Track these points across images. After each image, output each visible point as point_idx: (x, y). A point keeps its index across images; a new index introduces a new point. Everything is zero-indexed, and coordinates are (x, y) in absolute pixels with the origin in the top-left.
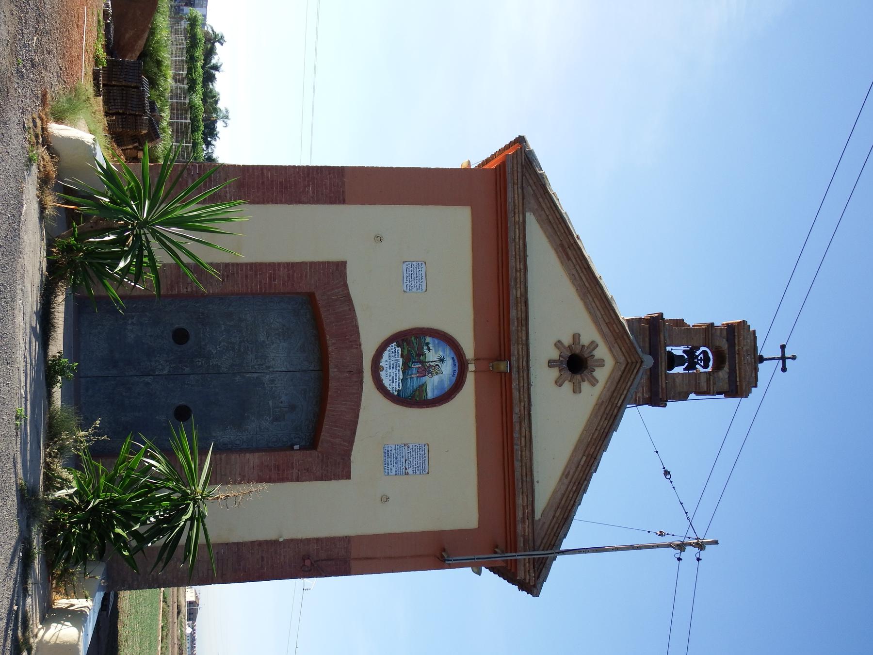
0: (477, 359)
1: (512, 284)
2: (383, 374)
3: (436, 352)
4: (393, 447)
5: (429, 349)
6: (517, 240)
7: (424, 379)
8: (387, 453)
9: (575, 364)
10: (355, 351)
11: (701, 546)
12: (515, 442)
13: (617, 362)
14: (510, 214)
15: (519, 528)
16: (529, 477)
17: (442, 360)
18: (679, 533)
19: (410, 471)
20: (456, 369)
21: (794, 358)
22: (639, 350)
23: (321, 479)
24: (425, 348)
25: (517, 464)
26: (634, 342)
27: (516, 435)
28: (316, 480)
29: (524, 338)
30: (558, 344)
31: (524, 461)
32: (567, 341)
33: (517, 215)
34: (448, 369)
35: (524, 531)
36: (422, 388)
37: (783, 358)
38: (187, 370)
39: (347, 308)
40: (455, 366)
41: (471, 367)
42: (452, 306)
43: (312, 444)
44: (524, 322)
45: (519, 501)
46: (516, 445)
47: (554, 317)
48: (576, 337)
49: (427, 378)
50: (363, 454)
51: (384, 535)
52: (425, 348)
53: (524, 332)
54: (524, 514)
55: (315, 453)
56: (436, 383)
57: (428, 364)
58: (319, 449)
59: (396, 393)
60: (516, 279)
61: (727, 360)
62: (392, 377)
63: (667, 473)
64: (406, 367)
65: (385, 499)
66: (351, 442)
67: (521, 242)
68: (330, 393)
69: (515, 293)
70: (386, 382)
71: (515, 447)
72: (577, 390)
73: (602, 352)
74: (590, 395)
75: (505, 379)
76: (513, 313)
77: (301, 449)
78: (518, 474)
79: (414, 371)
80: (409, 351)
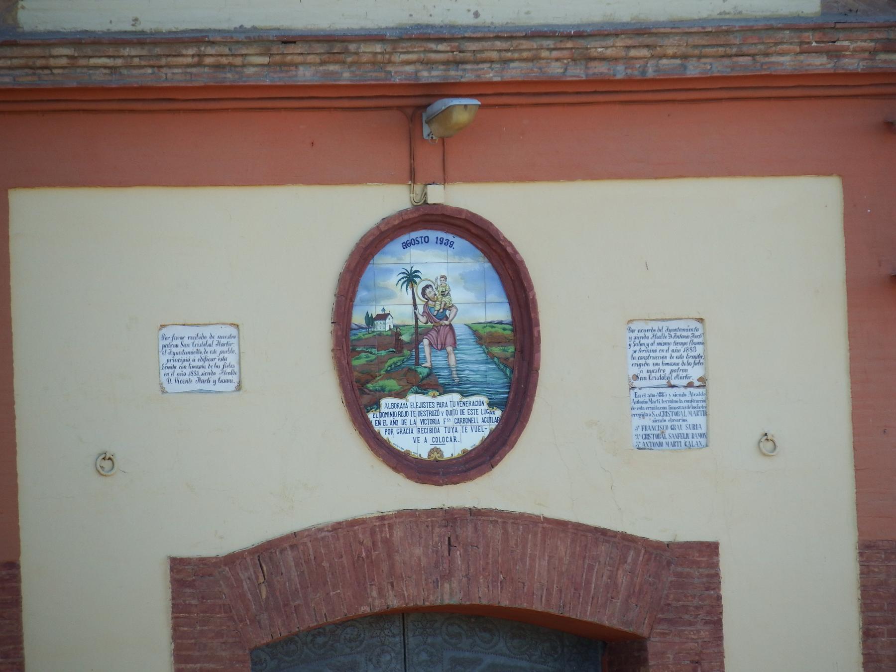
0: (412, 177)
1: (229, 77)
2: (450, 451)
3: (390, 296)
4: (637, 421)
5: (383, 317)
6: (119, 62)
7: (461, 332)
8: (651, 441)
10: (398, 533)
12: (636, 74)
14: (46, 80)
15: (852, 64)
16: (597, 48)
17: (411, 278)
19: (695, 373)
20: (433, 235)
23: (717, 624)
24: (381, 327)
25: (693, 69)
27: (620, 72)
28: (720, 638)
29: (378, 48)
31: (690, 51)
33: (52, 62)
34: (442, 263)
35: (863, 50)
36: (484, 337)
39: (290, 555)
40: (426, 240)
41: (437, 195)
44: (337, 48)
45: (785, 62)
46: (644, 72)
50: (651, 508)
51: (857, 447)
52: (381, 327)
53: (365, 48)
54: (818, 52)
55: (654, 645)
56: (470, 296)
57: (422, 320)
58: (644, 631)
59: (498, 413)
60: (218, 67)
62: (451, 424)
64: (429, 384)
65: (767, 443)
66: (627, 541)
67: (126, 51)
68: (505, 603)
69: (255, 68)
70: (471, 440)
71: (651, 73)
76: (305, 75)
78: (719, 68)
79: (439, 360)
80: (389, 374)
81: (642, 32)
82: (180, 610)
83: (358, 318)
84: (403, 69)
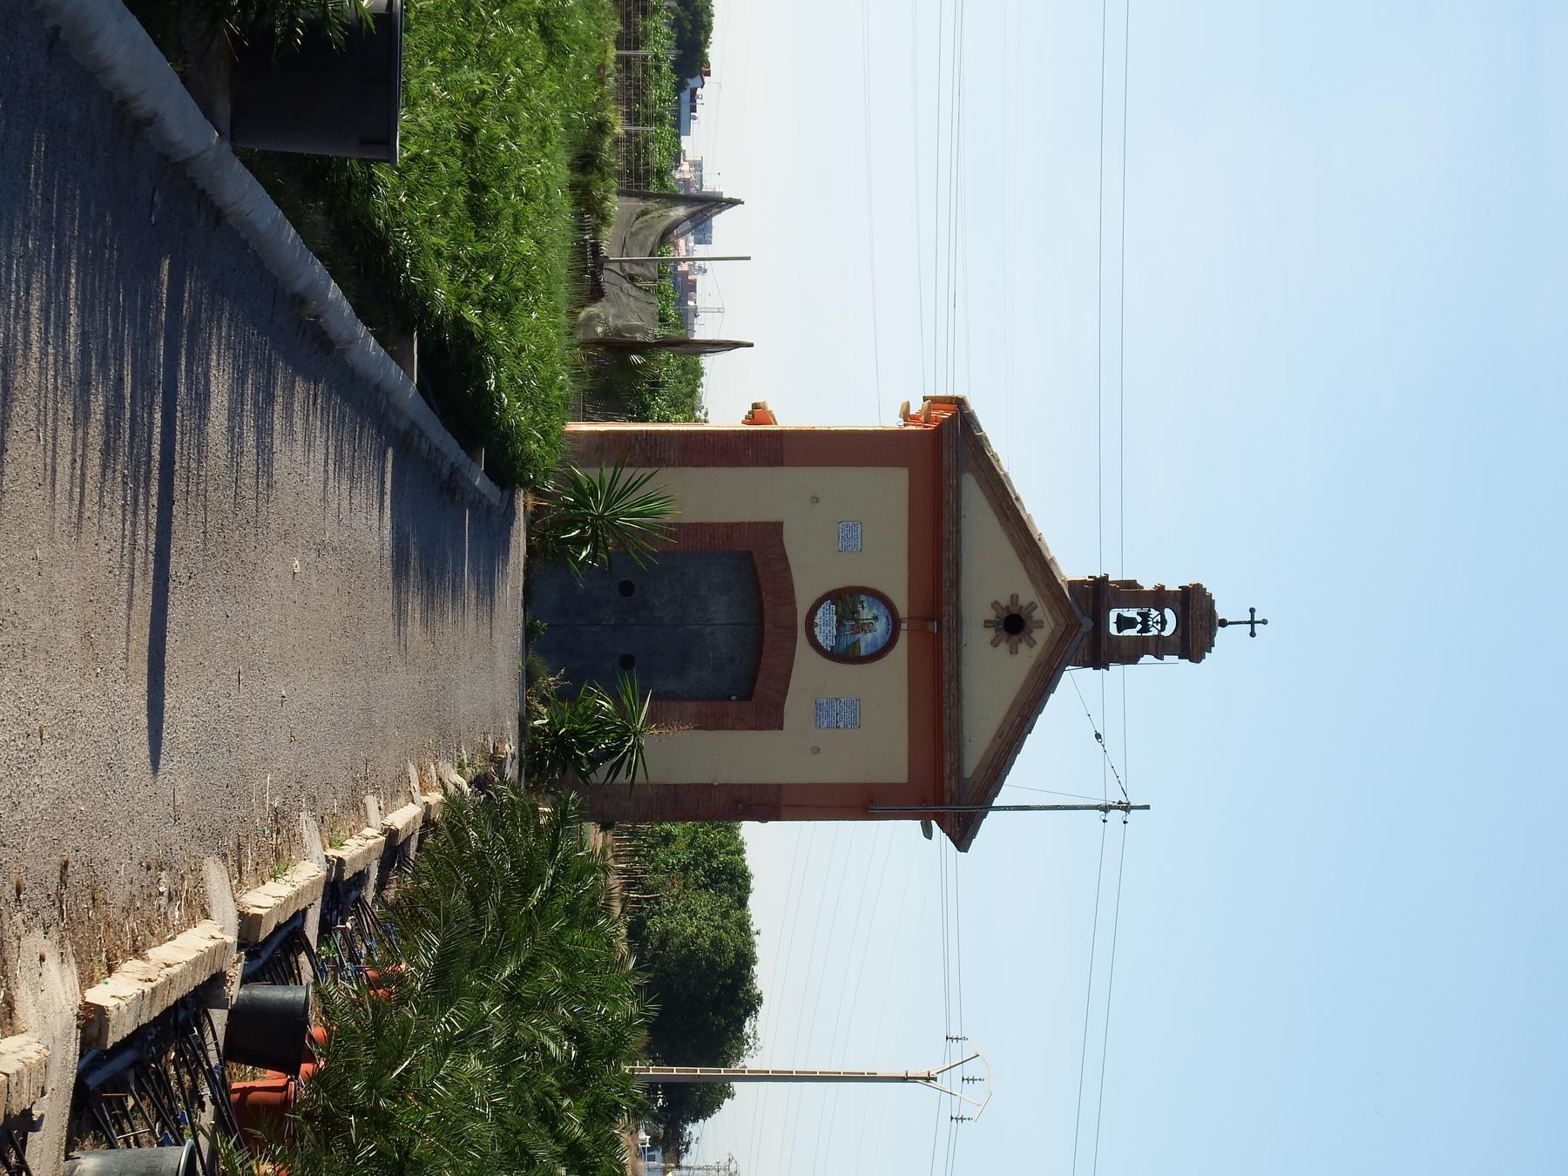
0: (910, 618)
2: (817, 630)
8: (818, 706)
9: (1013, 624)
11: (1127, 808)
13: (1057, 624)
17: (876, 618)
18: (1115, 797)
21: (1264, 622)
22: (1078, 613)
25: (945, 722)
26: (1075, 606)
27: (945, 694)
30: (995, 605)
32: (1004, 602)
34: (881, 627)
36: (856, 644)
37: (1252, 622)
38: (632, 621)
41: (904, 626)
42: (886, 566)
43: (748, 696)
45: (947, 757)
47: (988, 580)
48: (1014, 598)
49: (860, 636)
50: (796, 707)
61: (1192, 623)
63: (1098, 736)
64: (840, 624)
65: (816, 750)
70: (820, 639)
72: (1014, 651)
73: (1041, 613)
74: (1027, 656)
75: (937, 639)
76: (946, 574)
77: (739, 699)
81: (958, 699)
82: (765, 525)
83: (863, 597)
84: (947, 610)
